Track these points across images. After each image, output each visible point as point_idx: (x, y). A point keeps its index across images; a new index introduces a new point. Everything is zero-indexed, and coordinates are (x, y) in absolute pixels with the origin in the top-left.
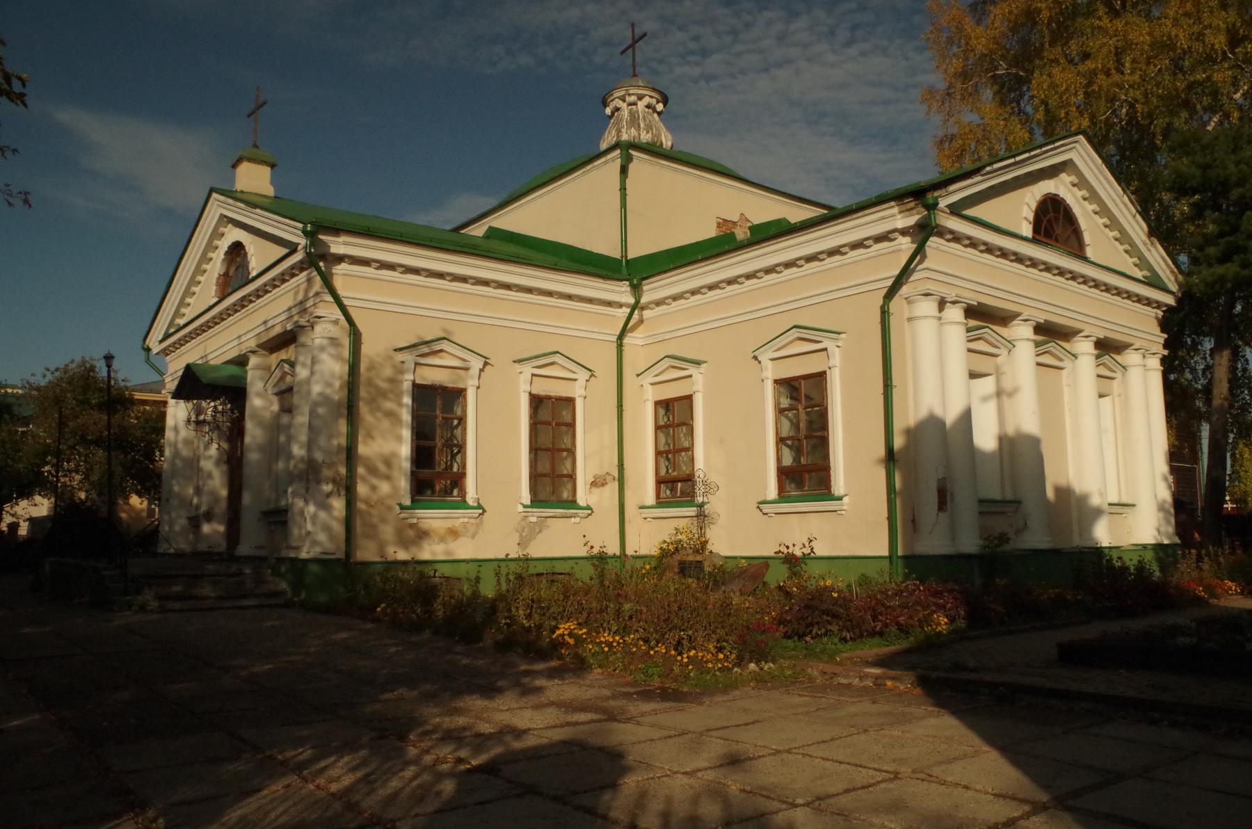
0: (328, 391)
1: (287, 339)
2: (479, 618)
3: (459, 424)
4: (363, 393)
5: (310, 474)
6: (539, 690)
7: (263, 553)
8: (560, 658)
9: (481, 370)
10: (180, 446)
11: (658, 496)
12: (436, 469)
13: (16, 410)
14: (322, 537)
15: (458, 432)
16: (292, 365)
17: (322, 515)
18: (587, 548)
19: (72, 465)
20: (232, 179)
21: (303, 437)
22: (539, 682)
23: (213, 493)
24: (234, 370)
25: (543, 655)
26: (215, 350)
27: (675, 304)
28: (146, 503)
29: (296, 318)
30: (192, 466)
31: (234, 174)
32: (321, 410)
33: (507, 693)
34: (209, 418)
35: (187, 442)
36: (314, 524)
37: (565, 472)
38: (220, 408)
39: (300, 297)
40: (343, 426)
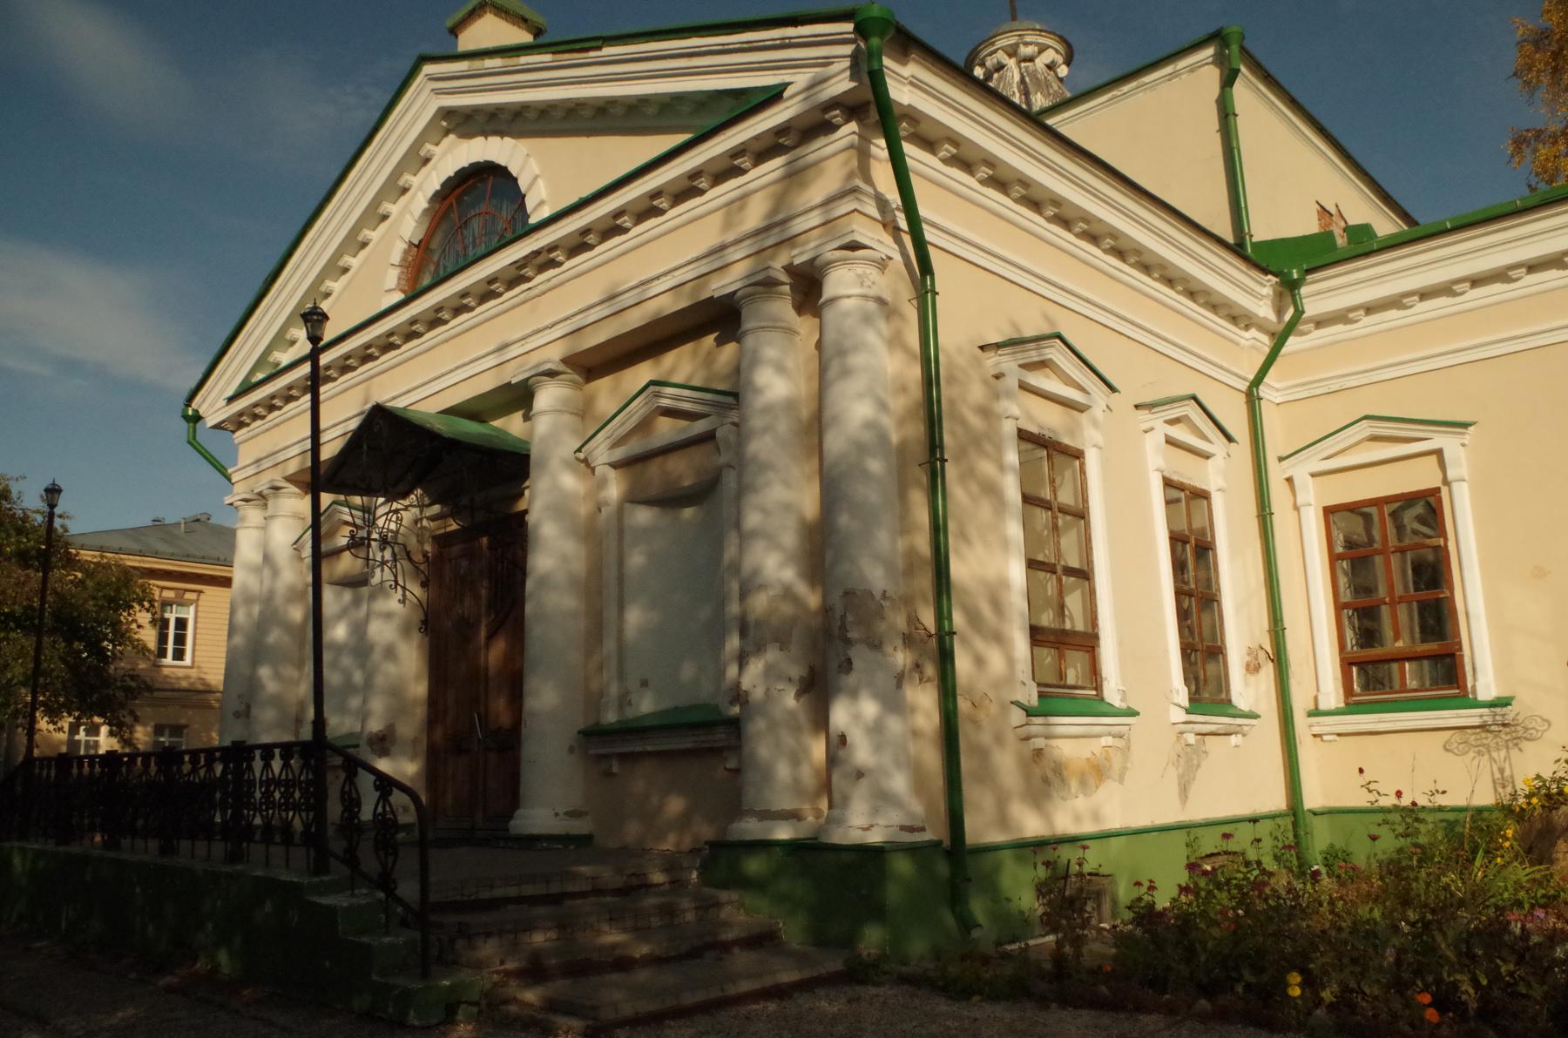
7: (580, 827)
11: (1348, 691)
17: (895, 725)
23: (396, 691)
26: (430, 380)
27: (1367, 320)
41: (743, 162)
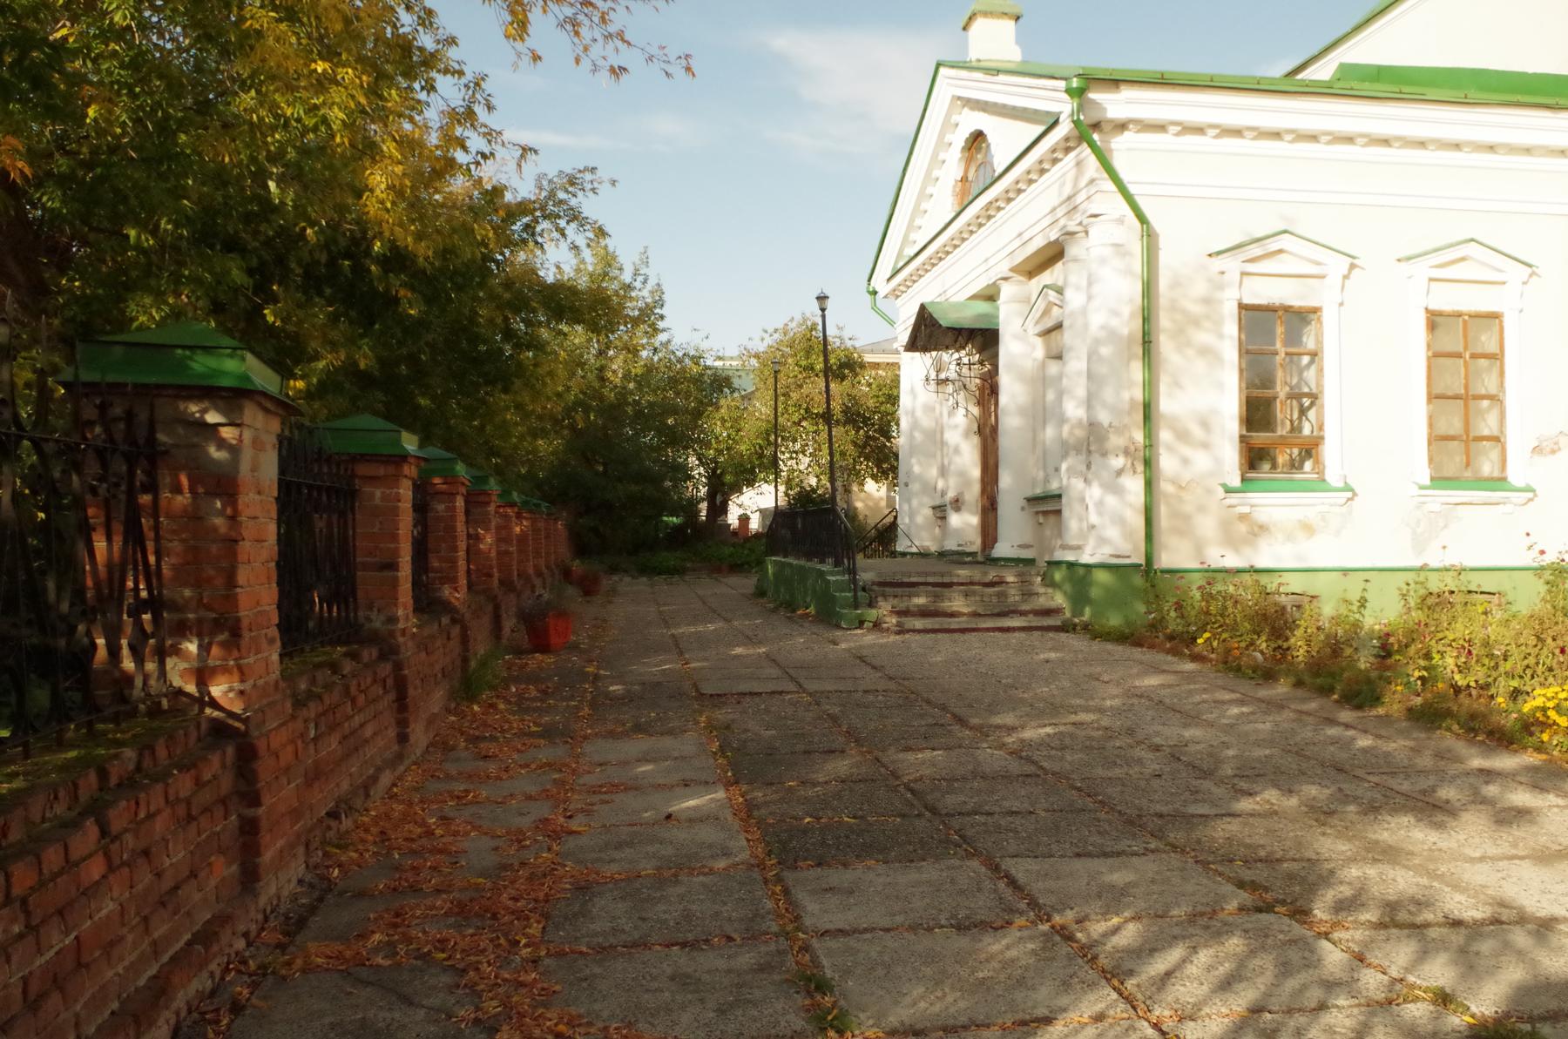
0: (1114, 322)
1: (1053, 255)
2: (1364, 662)
3: (1312, 362)
4: (1164, 321)
5: (1091, 442)
6: (1522, 815)
8: (1540, 748)
9: (1346, 277)
10: (919, 413)
12: (1272, 435)
13: (736, 383)
14: (1113, 533)
15: (1310, 375)
16: (1060, 291)
17: (1111, 501)
18: (1535, 553)
19: (798, 446)
20: (964, 46)
21: (1081, 391)
22: (1521, 797)
23: (962, 474)
24: (982, 307)
25: (1503, 739)
28: (884, 489)
29: (1062, 222)
30: (935, 438)
31: (966, 41)
32: (1105, 351)
33: (1466, 817)
34: (952, 375)
35: (929, 409)
36: (1100, 514)
37: (1486, 432)
38: (965, 360)
39: (1067, 191)
40: (1137, 371)
41: (1059, 155)
